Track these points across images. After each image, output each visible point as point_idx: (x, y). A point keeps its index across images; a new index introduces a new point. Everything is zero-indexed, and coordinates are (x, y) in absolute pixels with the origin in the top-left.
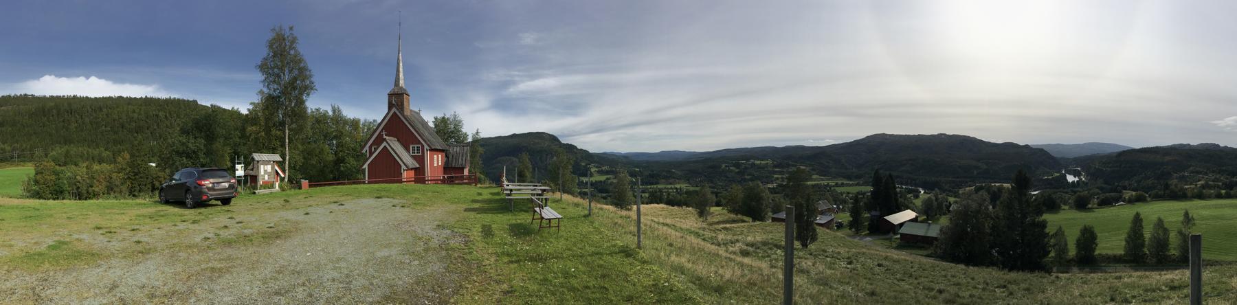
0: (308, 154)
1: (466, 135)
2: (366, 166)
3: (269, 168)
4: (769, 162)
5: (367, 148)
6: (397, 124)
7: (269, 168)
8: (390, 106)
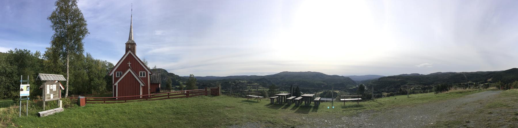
0: (76, 76)
2: (116, 84)
3: (54, 87)
4: (246, 81)
5: (113, 73)
6: (131, 60)
7: (54, 87)
8: (127, 50)
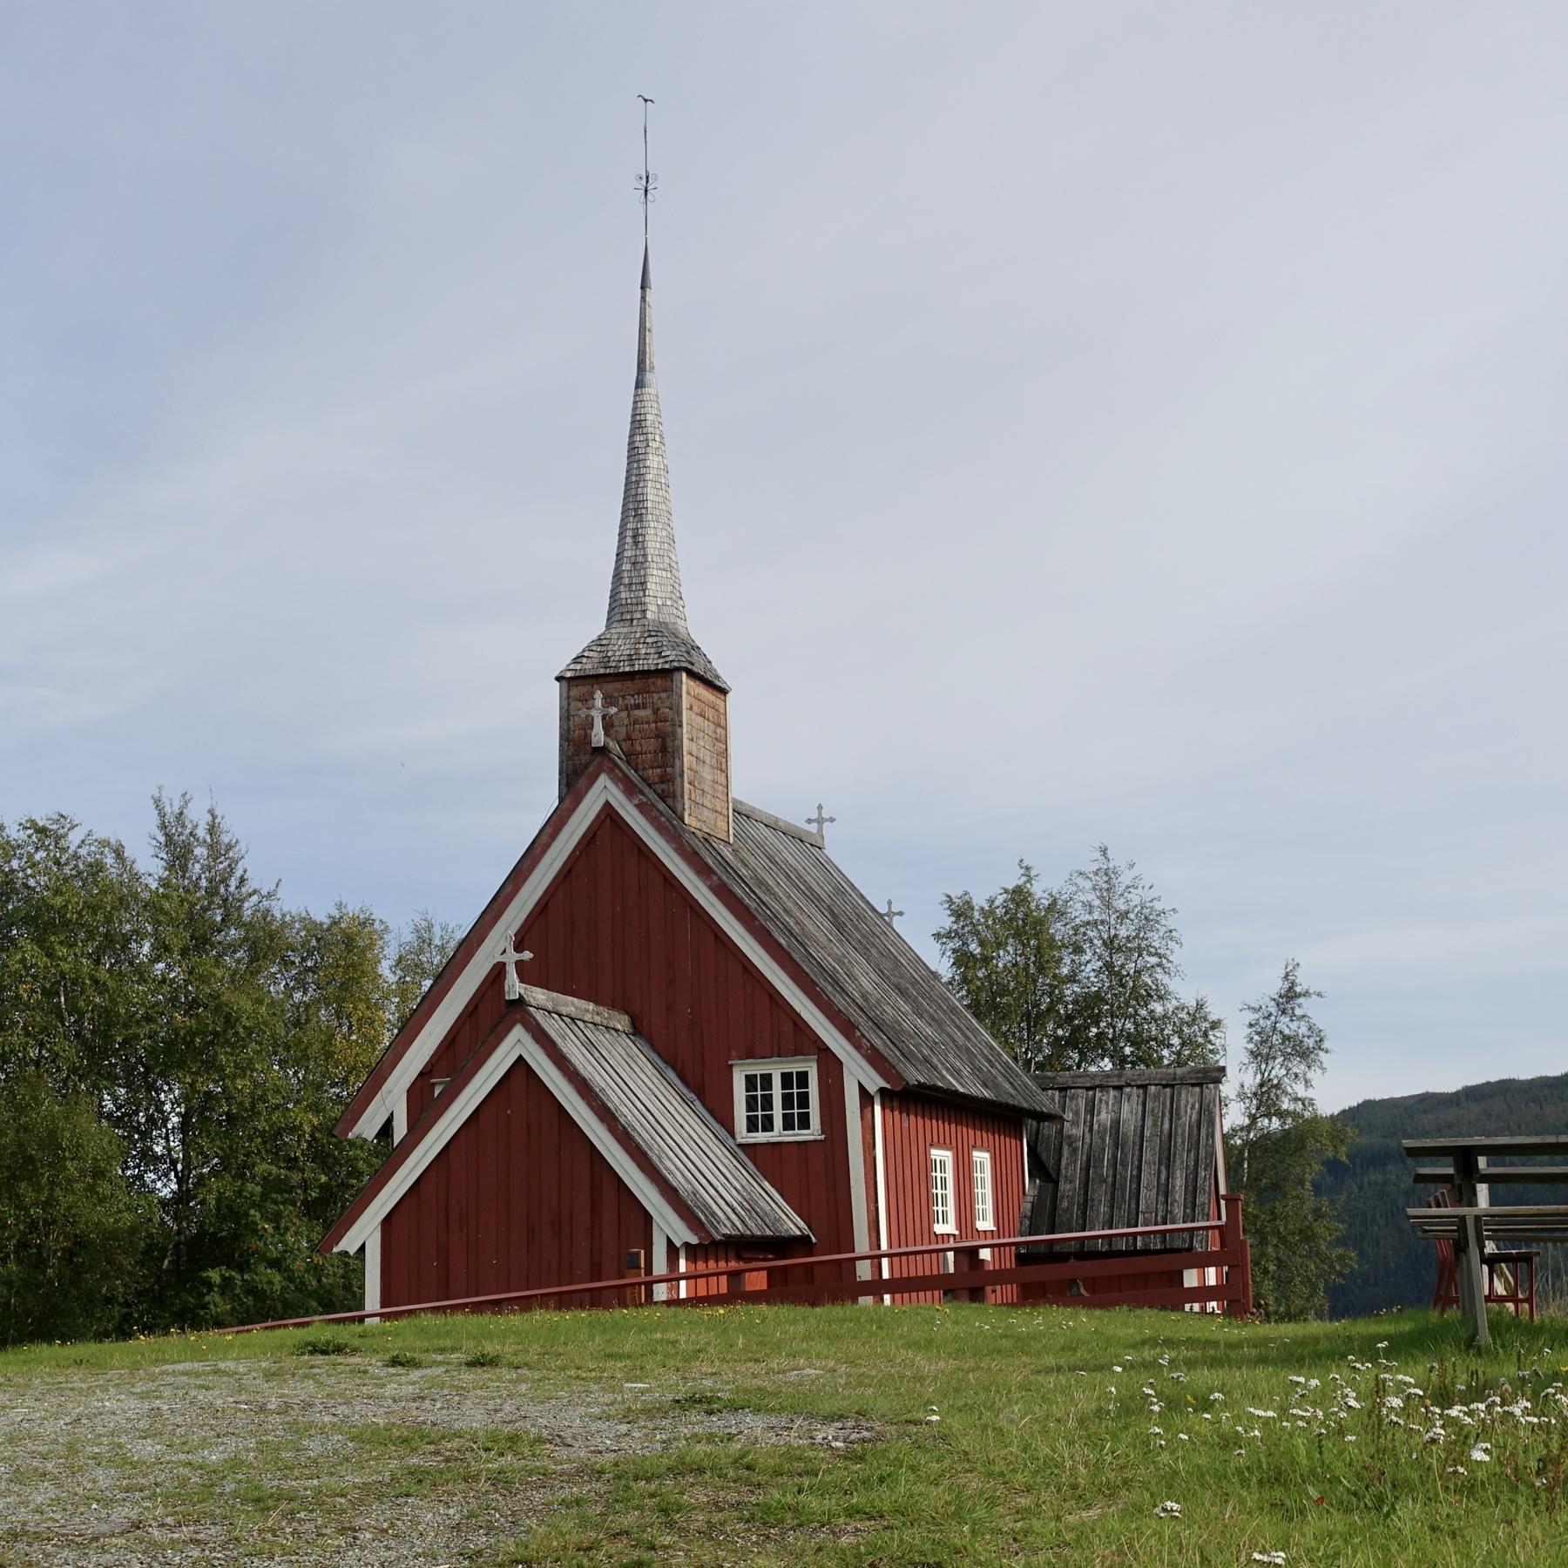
1: (1198, 1025)
2: (364, 1234)
8: (579, 763)
